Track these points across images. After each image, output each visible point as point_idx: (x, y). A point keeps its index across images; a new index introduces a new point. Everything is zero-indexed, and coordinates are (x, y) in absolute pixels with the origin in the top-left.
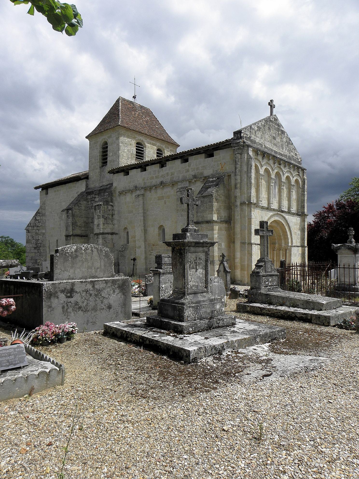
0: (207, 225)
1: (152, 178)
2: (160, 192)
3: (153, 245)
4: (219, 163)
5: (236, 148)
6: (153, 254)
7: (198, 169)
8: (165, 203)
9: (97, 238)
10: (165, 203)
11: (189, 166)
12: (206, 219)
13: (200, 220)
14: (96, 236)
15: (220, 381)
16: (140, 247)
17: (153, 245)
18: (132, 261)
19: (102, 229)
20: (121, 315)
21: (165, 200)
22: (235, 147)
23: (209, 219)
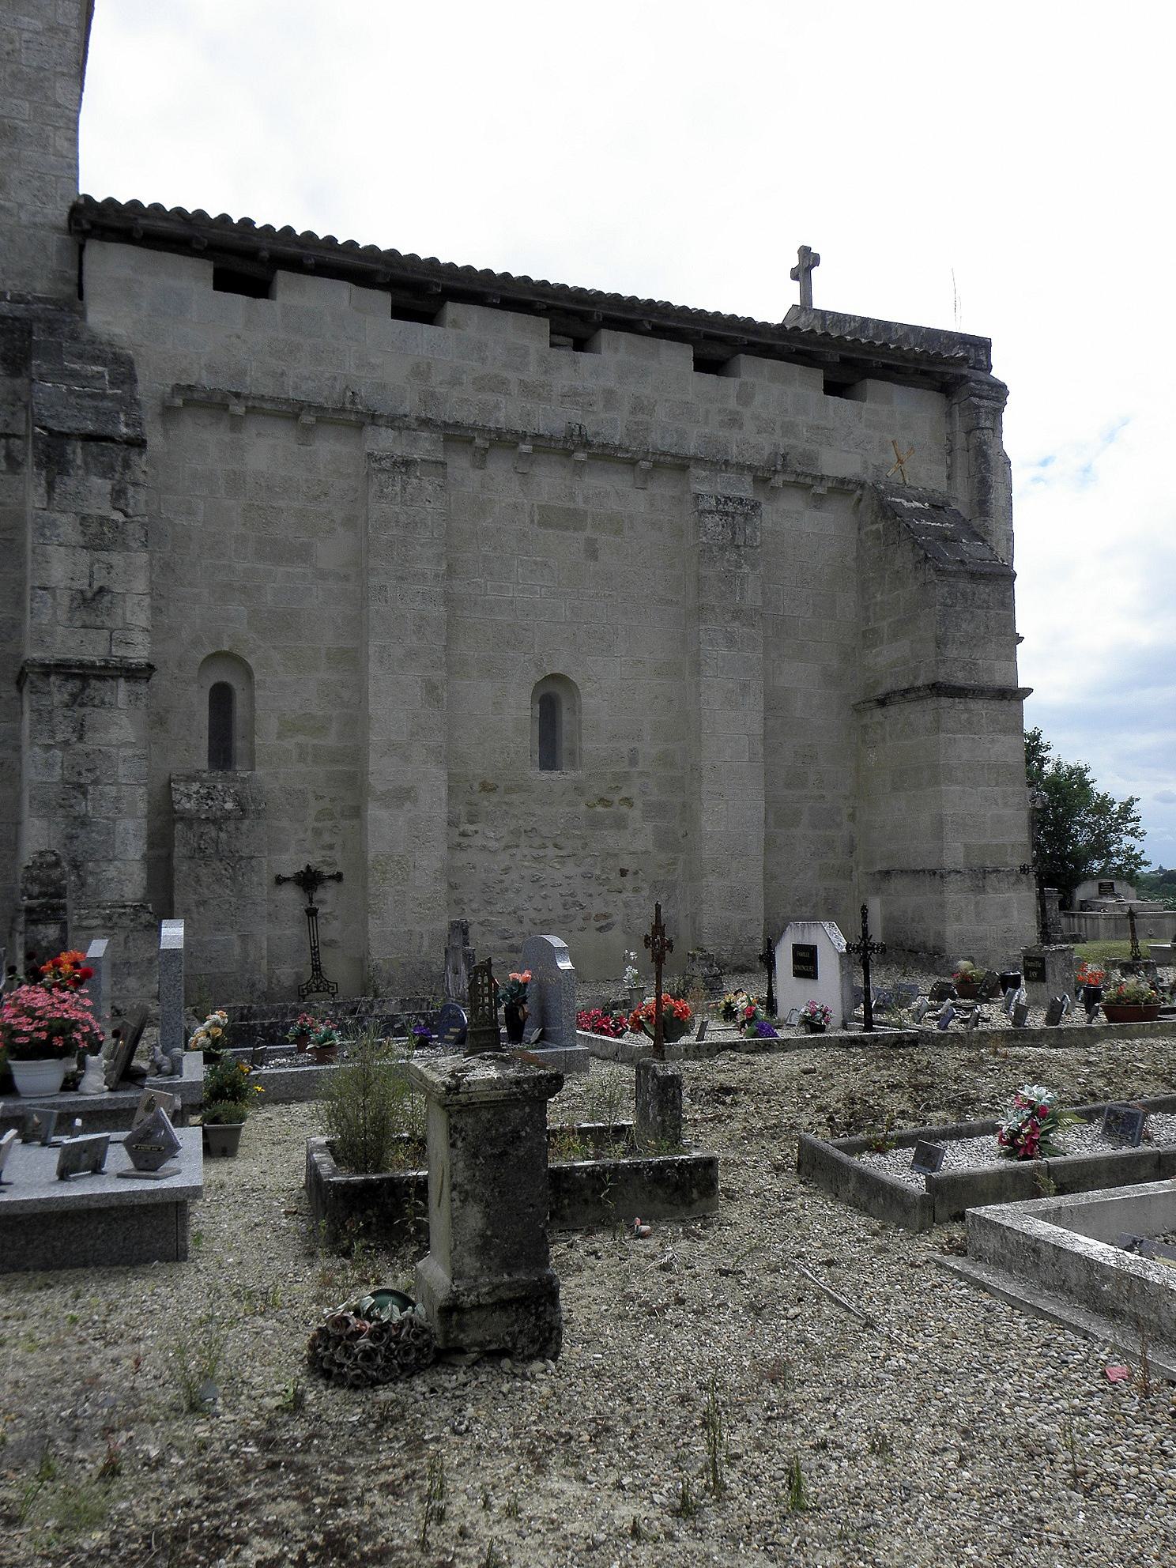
0: (995, 705)
1: (499, 385)
2: (551, 482)
3: (487, 788)
4: (890, 438)
5: (985, 402)
6: (478, 841)
7: (789, 429)
8: (592, 553)
9: (75, 700)
10: (592, 553)
11: (745, 398)
12: (985, 680)
13: (960, 678)
14: (58, 692)
15: (351, 1461)
16: (403, 796)
17: (487, 788)
18: (291, 896)
19: (138, 637)
20: (1047, 1253)
21: (588, 533)
22: (981, 397)
23: (999, 681)
